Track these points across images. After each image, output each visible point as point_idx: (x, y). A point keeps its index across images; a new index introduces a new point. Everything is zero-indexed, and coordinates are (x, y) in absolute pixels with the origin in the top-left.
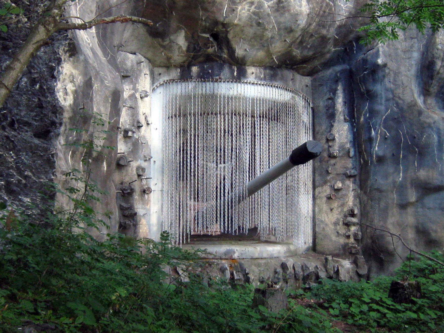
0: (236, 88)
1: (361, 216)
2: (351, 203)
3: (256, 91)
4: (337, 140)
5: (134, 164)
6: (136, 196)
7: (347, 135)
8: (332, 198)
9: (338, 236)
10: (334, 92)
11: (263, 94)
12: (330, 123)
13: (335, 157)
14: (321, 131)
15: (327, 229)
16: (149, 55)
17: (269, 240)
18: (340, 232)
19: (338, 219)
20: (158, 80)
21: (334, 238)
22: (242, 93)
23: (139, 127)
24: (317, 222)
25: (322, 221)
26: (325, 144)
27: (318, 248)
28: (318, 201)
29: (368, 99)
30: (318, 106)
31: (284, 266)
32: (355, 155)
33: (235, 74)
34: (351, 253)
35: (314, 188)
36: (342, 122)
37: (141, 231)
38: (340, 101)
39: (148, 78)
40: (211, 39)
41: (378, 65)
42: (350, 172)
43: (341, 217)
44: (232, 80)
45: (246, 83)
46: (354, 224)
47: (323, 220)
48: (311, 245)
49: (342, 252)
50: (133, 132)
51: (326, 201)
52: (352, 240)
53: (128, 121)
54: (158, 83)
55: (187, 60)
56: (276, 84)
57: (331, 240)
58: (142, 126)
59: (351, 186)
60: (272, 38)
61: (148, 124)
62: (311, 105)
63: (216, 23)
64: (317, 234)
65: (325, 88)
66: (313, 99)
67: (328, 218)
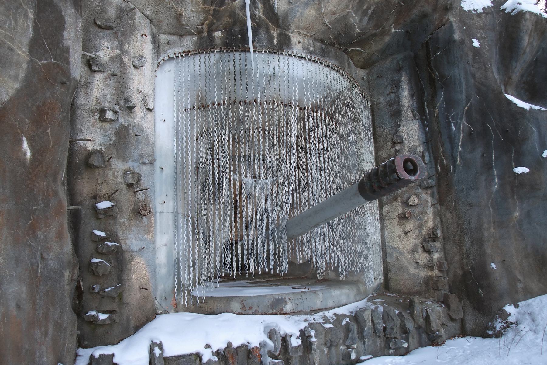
0: (276, 62)
1: (444, 239)
3: (305, 69)
4: (406, 142)
7: (418, 136)
8: (407, 218)
9: (417, 268)
10: (397, 85)
11: (314, 75)
12: (395, 122)
14: (384, 133)
15: (402, 258)
19: (415, 245)
20: (165, 51)
21: (412, 270)
24: (389, 251)
25: (395, 249)
26: (391, 149)
27: (392, 284)
28: (387, 223)
29: (442, 88)
30: (379, 103)
32: (430, 161)
33: (275, 41)
36: (411, 120)
37: (134, 276)
38: (405, 93)
41: (454, 41)
42: (427, 182)
43: (418, 241)
44: (270, 50)
45: (291, 56)
47: (396, 246)
48: (382, 281)
49: (424, 288)
51: (399, 222)
52: (436, 272)
53: (108, 96)
54: (166, 55)
55: (206, 19)
57: (409, 274)
58: (134, 107)
59: (429, 200)
62: (369, 103)
64: (389, 267)
65: (385, 80)
66: (371, 96)
67: (403, 244)
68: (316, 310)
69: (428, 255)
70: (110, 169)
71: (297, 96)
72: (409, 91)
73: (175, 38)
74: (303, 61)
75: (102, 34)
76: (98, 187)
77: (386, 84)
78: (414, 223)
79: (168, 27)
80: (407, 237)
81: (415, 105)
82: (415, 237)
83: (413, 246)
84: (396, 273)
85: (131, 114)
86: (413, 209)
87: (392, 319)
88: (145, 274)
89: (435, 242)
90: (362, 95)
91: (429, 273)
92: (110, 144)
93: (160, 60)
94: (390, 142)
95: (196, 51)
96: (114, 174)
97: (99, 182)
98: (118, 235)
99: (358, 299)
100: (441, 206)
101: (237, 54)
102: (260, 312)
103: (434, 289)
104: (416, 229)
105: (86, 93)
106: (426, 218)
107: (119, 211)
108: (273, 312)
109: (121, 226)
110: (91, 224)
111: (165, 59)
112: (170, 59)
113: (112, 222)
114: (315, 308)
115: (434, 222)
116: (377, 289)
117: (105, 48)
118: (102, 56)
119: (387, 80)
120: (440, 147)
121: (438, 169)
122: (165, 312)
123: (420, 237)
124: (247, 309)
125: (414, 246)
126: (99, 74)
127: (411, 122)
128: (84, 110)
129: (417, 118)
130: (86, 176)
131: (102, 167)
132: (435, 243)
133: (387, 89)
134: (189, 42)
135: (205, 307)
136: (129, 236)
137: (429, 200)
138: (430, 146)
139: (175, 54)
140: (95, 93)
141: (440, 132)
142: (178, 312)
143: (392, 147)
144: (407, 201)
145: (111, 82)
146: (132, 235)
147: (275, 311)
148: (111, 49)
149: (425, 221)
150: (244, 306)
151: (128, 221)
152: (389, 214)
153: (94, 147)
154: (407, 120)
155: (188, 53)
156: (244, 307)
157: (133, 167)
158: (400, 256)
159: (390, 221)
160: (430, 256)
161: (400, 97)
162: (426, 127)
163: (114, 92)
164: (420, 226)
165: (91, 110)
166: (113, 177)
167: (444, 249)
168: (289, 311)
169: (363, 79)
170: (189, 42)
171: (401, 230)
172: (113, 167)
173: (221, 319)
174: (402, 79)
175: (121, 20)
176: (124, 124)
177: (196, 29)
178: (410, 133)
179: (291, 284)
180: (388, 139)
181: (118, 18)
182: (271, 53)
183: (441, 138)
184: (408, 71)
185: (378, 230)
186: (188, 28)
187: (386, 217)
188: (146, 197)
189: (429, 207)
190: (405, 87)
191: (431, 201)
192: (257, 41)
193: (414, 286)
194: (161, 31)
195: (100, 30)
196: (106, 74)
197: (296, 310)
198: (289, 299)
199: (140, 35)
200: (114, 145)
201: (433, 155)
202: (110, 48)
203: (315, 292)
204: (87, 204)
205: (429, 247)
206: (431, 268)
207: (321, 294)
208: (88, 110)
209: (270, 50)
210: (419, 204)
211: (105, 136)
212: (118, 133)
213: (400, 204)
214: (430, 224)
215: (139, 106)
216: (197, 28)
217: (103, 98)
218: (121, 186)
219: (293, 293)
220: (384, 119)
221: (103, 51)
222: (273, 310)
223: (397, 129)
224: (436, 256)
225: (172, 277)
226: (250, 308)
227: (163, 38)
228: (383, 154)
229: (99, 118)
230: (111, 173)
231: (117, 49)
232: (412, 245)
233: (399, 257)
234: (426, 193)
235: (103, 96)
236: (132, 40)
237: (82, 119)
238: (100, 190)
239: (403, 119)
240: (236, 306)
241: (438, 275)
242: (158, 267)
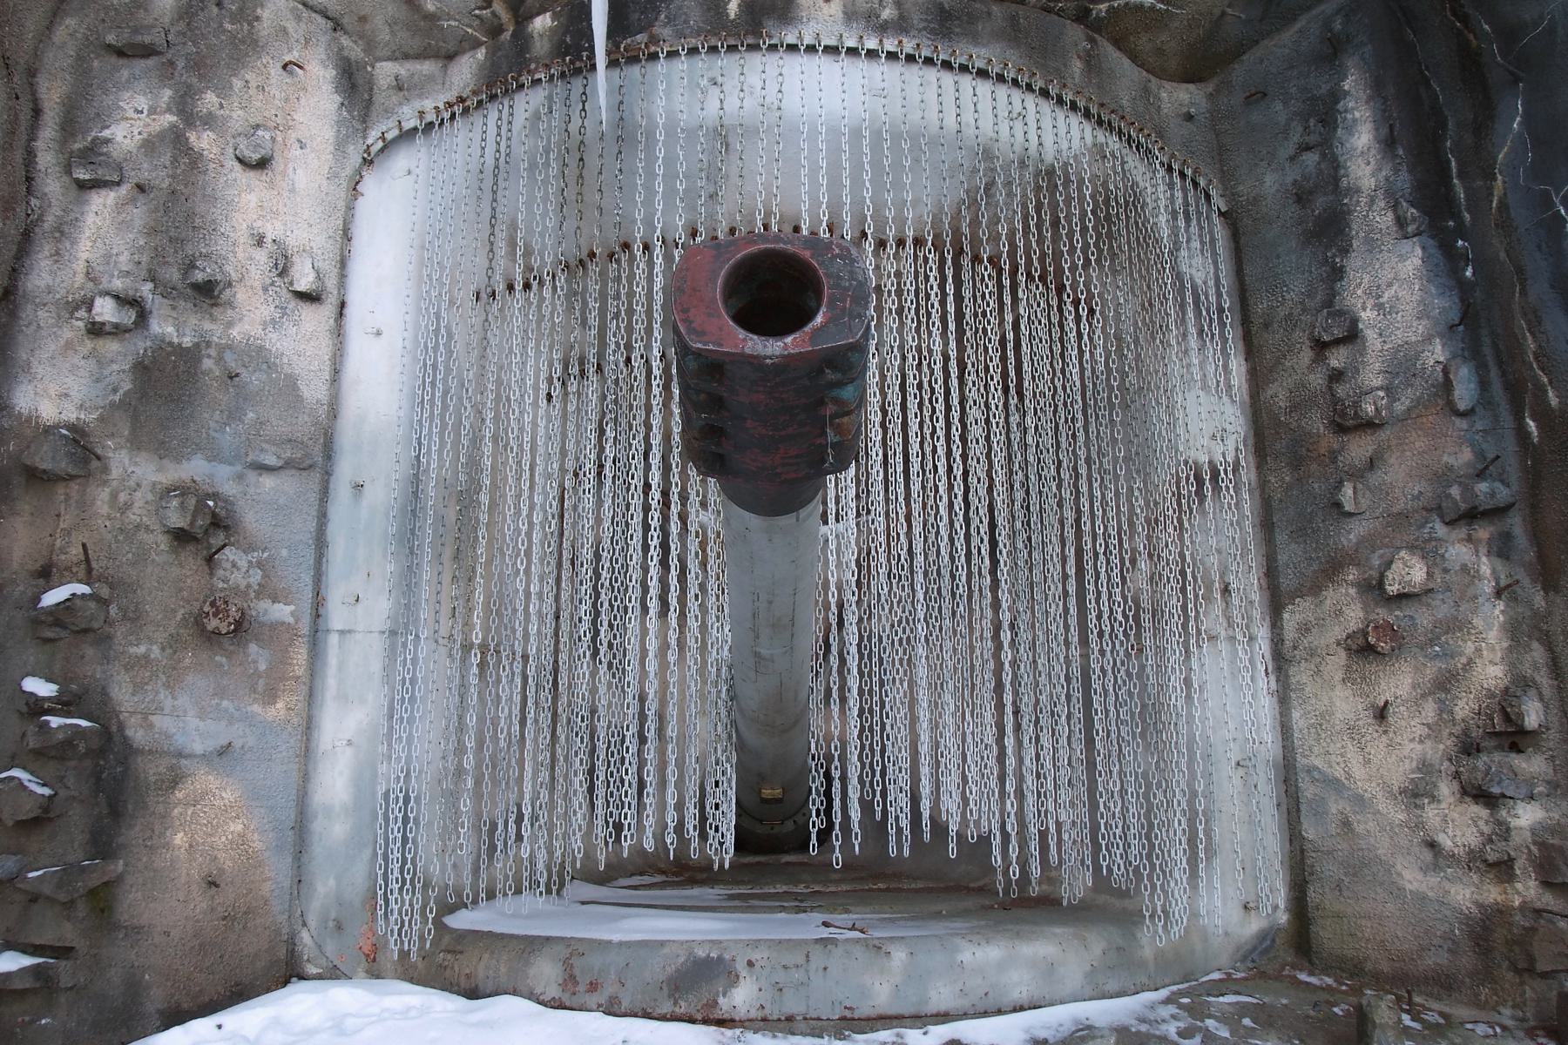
4: (1371, 335)
7: (1421, 302)
9: (1436, 867)
13: (1370, 425)
14: (1282, 312)
18: (1446, 842)
19: (1425, 767)
20: (388, 112)
21: (1412, 878)
24: (1308, 790)
25: (1334, 784)
26: (1311, 369)
27: (1325, 934)
28: (1300, 674)
29: (1517, 80)
35: (1276, 605)
37: (179, 839)
42: (1466, 489)
43: (1438, 751)
45: (792, 48)
47: (1338, 773)
48: (1283, 918)
49: (1467, 961)
51: (1348, 669)
52: (1527, 889)
53: (124, 258)
54: (392, 123)
57: (1397, 892)
59: (1485, 569)
62: (1219, 202)
65: (1279, 106)
66: (1227, 178)
67: (1367, 762)
68: (868, 1019)
69: (1484, 813)
70: (105, 483)
71: (909, 222)
72: (1377, 129)
73: (427, 67)
74: (845, 61)
75: (125, 73)
76: (59, 541)
78: (1416, 668)
79: (393, 33)
80: (1385, 732)
81: (1404, 181)
82: (1420, 731)
83: (1413, 772)
84: (1339, 887)
85: (216, 311)
86: (1409, 609)
88: (242, 836)
89: (1520, 751)
91: (1493, 894)
92: (112, 404)
94: (1307, 342)
96: (114, 496)
97: (62, 526)
98: (113, 695)
99: (1112, 986)
100: (1551, 594)
102: (625, 1005)
103: (1518, 971)
104: (1423, 696)
105: (57, 253)
106: (1469, 648)
107: (125, 617)
108: (677, 1010)
109: (128, 668)
110: (24, 657)
111: (389, 136)
112: (407, 135)
113: (90, 652)
114: (864, 1010)
115: (1512, 666)
116: (1254, 948)
117: (130, 113)
118: (119, 138)
120: (1524, 337)
121: (1529, 434)
122: (333, 973)
123: (1445, 733)
124: (581, 988)
125: (1419, 769)
126: (103, 192)
127: (1389, 251)
128: (45, 305)
129: (1411, 229)
130: (27, 507)
131: (72, 477)
132: (1517, 761)
133: (1286, 139)
134: (465, 72)
135: (452, 968)
136: (168, 703)
137: (1485, 569)
138: (1486, 340)
139: (422, 113)
140: (85, 250)
141: (1520, 270)
142: (378, 977)
143: (1314, 361)
144: (1382, 577)
145: (139, 214)
146: (183, 700)
147: (683, 1008)
148: (148, 115)
149: (1464, 660)
150: (572, 978)
151: (169, 651)
152: (1310, 639)
153: (62, 416)
154: (1371, 245)
155: (462, 107)
156: (570, 980)
157: (211, 476)
158: (1355, 813)
159: (1313, 667)
160: (1492, 814)
161: (1341, 159)
162: (1462, 264)
163: (142, 243)
164: (1445, 684)
165: (68, 302)
166: (111, 507)
168: (741, 1014)
170: (465, 72)
171: (1360, 705)
172: (115, 473)
173: (475, 1017)
174: (1346, 88)
175: (188, 24)
176: (176, 340)
177: (477, 22)
178: (1386, 295)
179: (858, 909)
180: (1297, 333)
181: (181, 18)
183: (1526, 294)
185: (1266, 706)
186: (453, 23)
187: (1295, 648)
188: (265, 576)
189: (1480, 600)
190: (1357, 114)
191: (1494, 571)
192: (666, 17)
194: (379, 53)
195: (121, 61)
196: (124, 190)
197: (774, 1012)
198: (750, 964)
199: (279, 65)
200: (124, 405)
201: (1504, 374)
202: (145, 112)
203: (877, 948)
204: (17, 594)
205: (1480, 776)
206: (1502, 869)
207: (899, 955)
208: (57, 303)
210: (1431, 586)
211: (98, 381)
212: (143, 369)
213: (1352, 591)
214: (1492, 673)
215: (257, 284)
216: (477, 16)
217: (108, 264)
218: (148, 538)
219: (780, 942)
220: (1278, 257)
221: (123, 123)
222: (675, 1003)
223: (1332, 289)
225: (367, 853)
226: (593, 987)
227: (386, 71)
228: (1278, 393)
230: (104, 494)
231: (169, 110)
232: (1408, 765)
233: (1352, 818)
234: (1469, 539)
235: (107, 257)
236: (237, 84)
237: (36, 331)
239: (1355, 244)
240: (546, 972)
241: (1538, 905)
242: (320, 817)
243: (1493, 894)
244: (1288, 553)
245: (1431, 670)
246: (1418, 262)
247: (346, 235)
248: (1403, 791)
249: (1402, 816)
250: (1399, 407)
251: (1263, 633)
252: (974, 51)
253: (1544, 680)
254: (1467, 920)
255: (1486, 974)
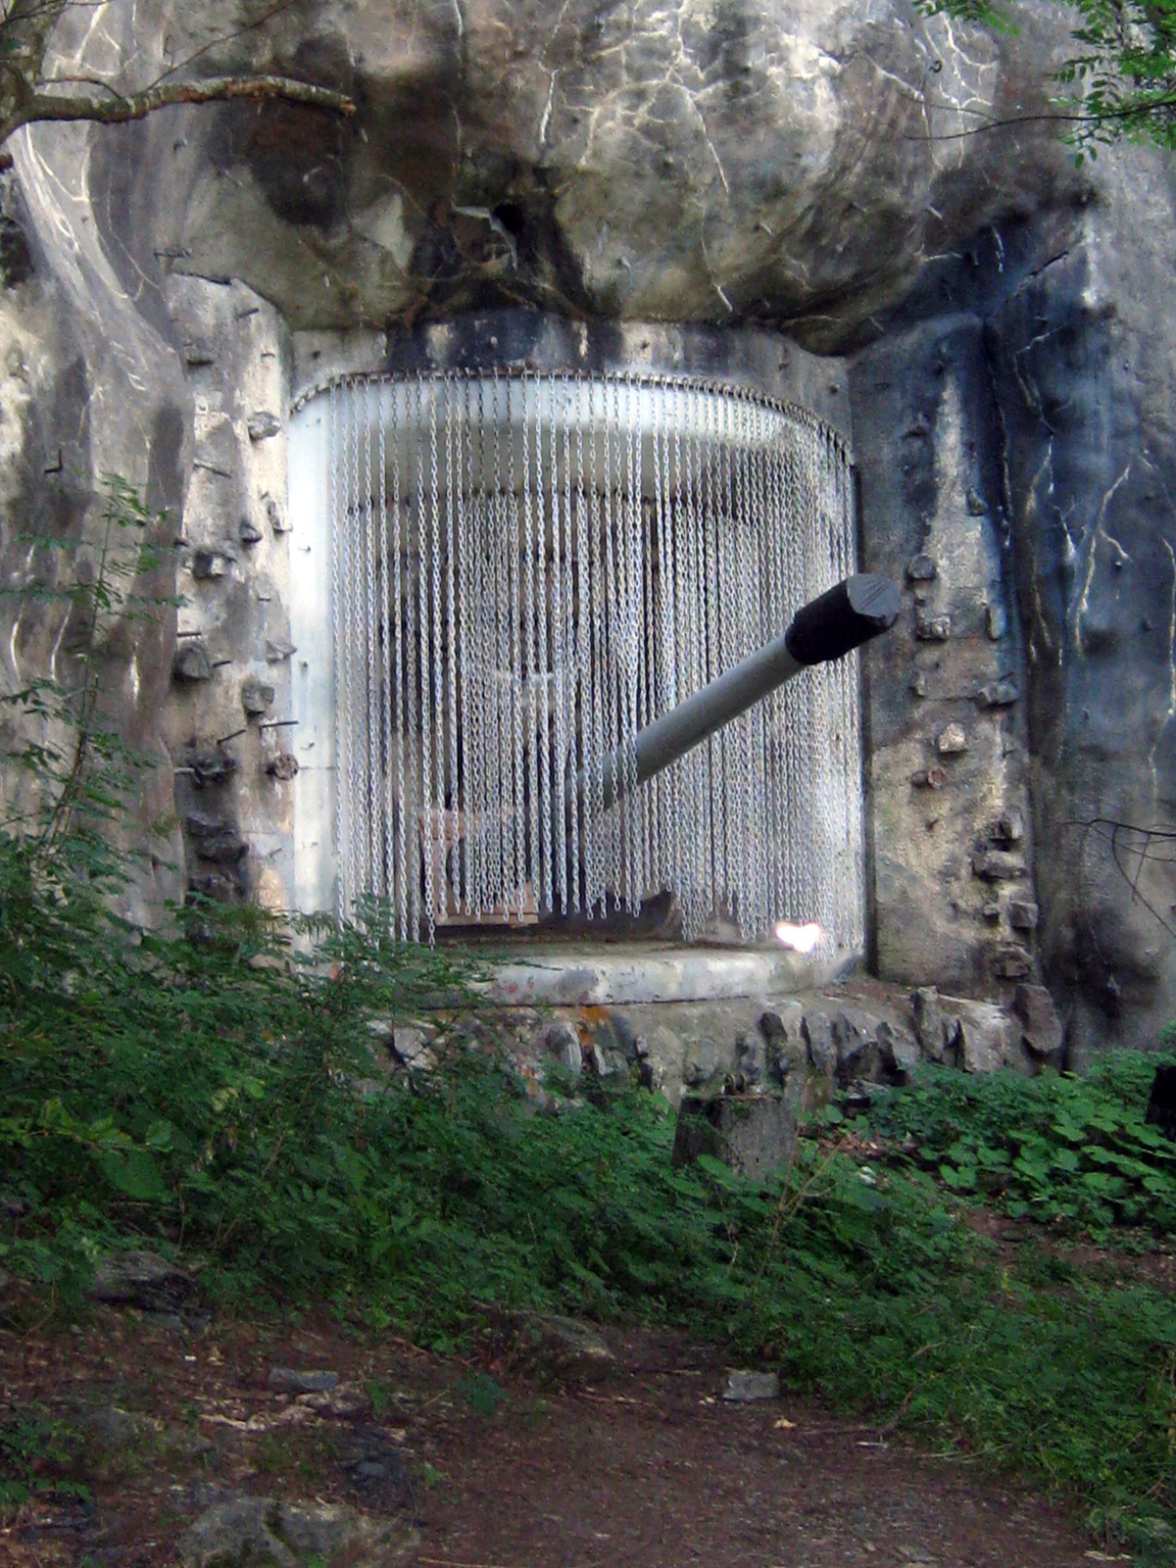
0: (585, 398)
1: (1035, 845)
2: (997, 802)
4: (944, 578)
5: (234, 675)
6: (244, 788)
7: (978, 561)
8: (930, 786)
10: (930, 409)
11: (681, 419)
12: (919, 519)
13: (938, 640)
14: (887, 548)
16: (278, 287)
17: (711, 938)
18: (962, 904)
19: (954, 859)
21: (941, 925)
22: (691, 426)
23: (249, 543)
24: (881, 871)
25: (898, 868)
27: (887, 960)
28: (881, 798)
31: (769, 1026)
32: (1008, 632)
34: (1002, 978)
35: (867, 749)
36: (962, 516)
39: (275, 368)
40: (496, 227)
41: (1085, 312)
43: (963, 851)
44: (571, 372)
45: (623, 380)
46: (1010, 875)
47: (901, 861)
48: (861, 952)
49: (970, 973)
50: (229, 561)
51: (912, 796)
52: (1004, 931)
56: (728, 383)
57: (931, 933)
59: (998, 739)
60: (712, 218)
61: (278, 532)
62: (850, 459)
63: (514, 167)
65: (897, 395)
77: (899, 405)
81: (975, 478)
87: (856, 1033)
90: (828, 438)
91: (987, 934)
93: (297, 399)
95: (384, 372)
101: (487, 386)
112: (319, 393)
119: (903, 397)
144: (937, 741)
167: (1032, 874)
169: (834, 391)
182: (571, 378)
184: (963, 374)
185: (856, 817)
193: (946, 967)
206: (992, 920)
209: (571, 372)
224: (1008, 890)
229: (194, 572)
238: (200, 729)
243: (987, 934)
244: (878, 715)
245: (961, 802)
246: (978, 535)
247: (286, 483)
248: (940, 872)
249: (937, 888)
250: (957, 630)
251: (856, 766)
252: (725, 380)
253: (1024, 807)
254: (970, 949)
255: (980, 980)
